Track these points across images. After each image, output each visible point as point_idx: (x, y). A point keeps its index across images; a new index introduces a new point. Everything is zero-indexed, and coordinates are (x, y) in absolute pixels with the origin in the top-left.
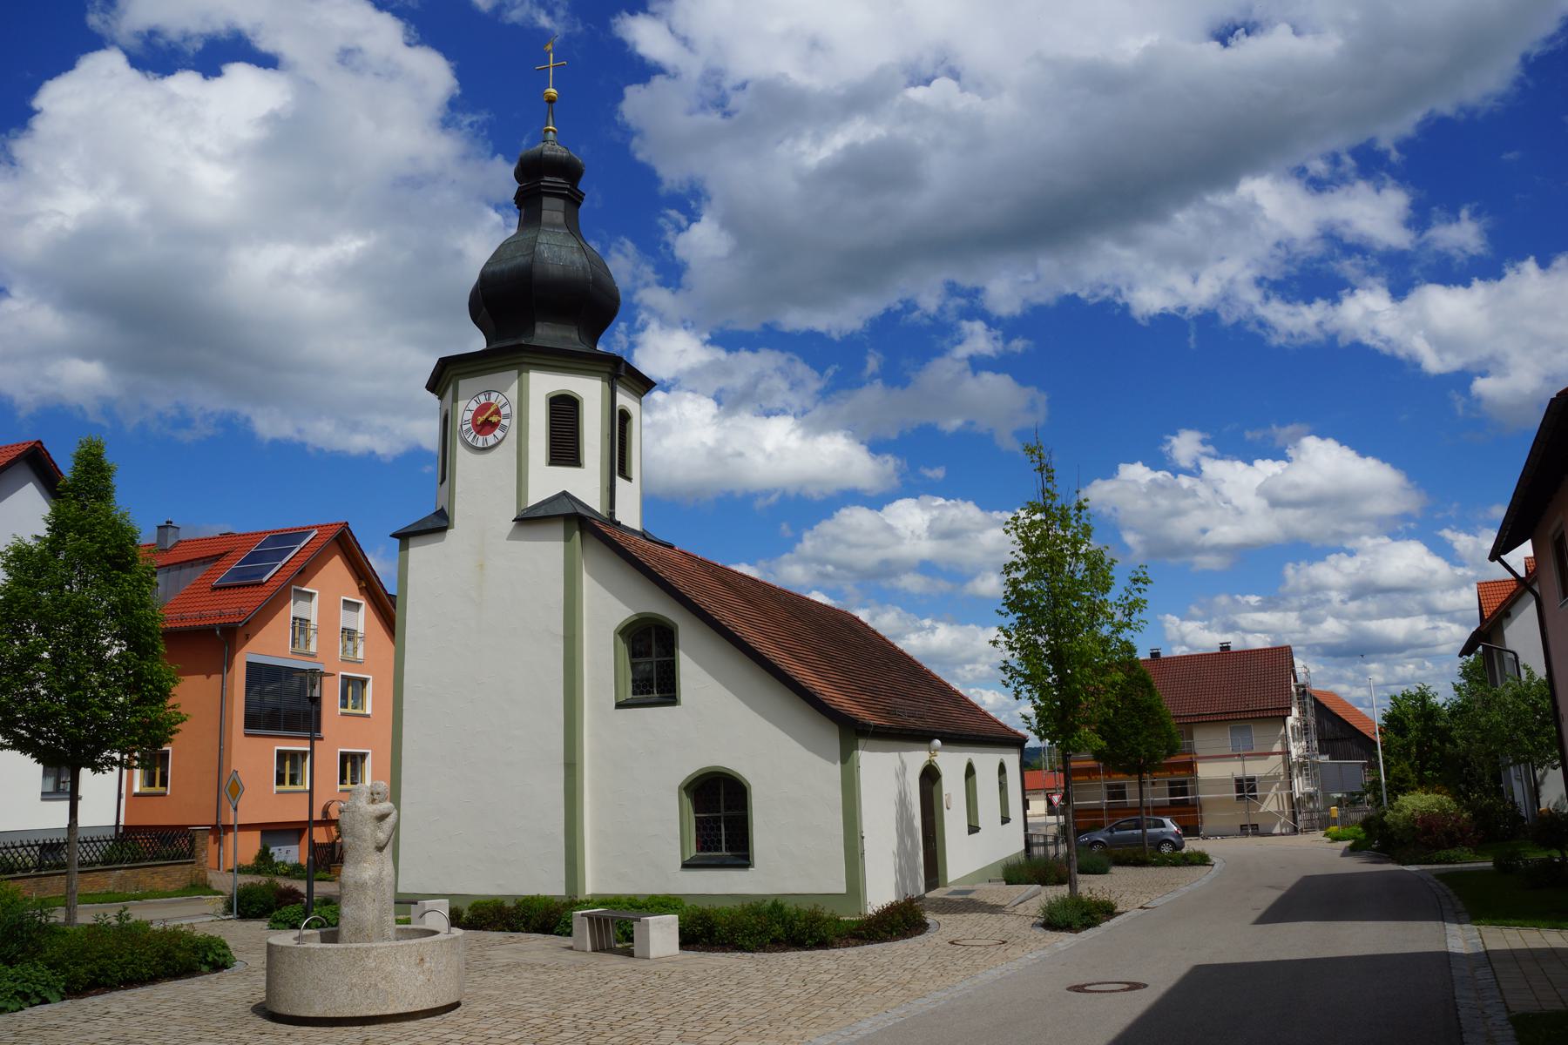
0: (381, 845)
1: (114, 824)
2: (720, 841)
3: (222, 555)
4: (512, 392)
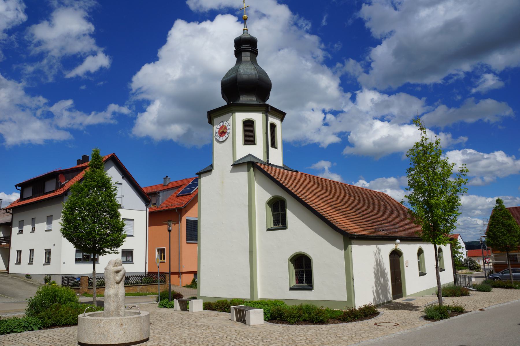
0: (118, 282)
1: (145, 271)
2: (303, 280)
3: (181, 186)
4: (230, 121)
